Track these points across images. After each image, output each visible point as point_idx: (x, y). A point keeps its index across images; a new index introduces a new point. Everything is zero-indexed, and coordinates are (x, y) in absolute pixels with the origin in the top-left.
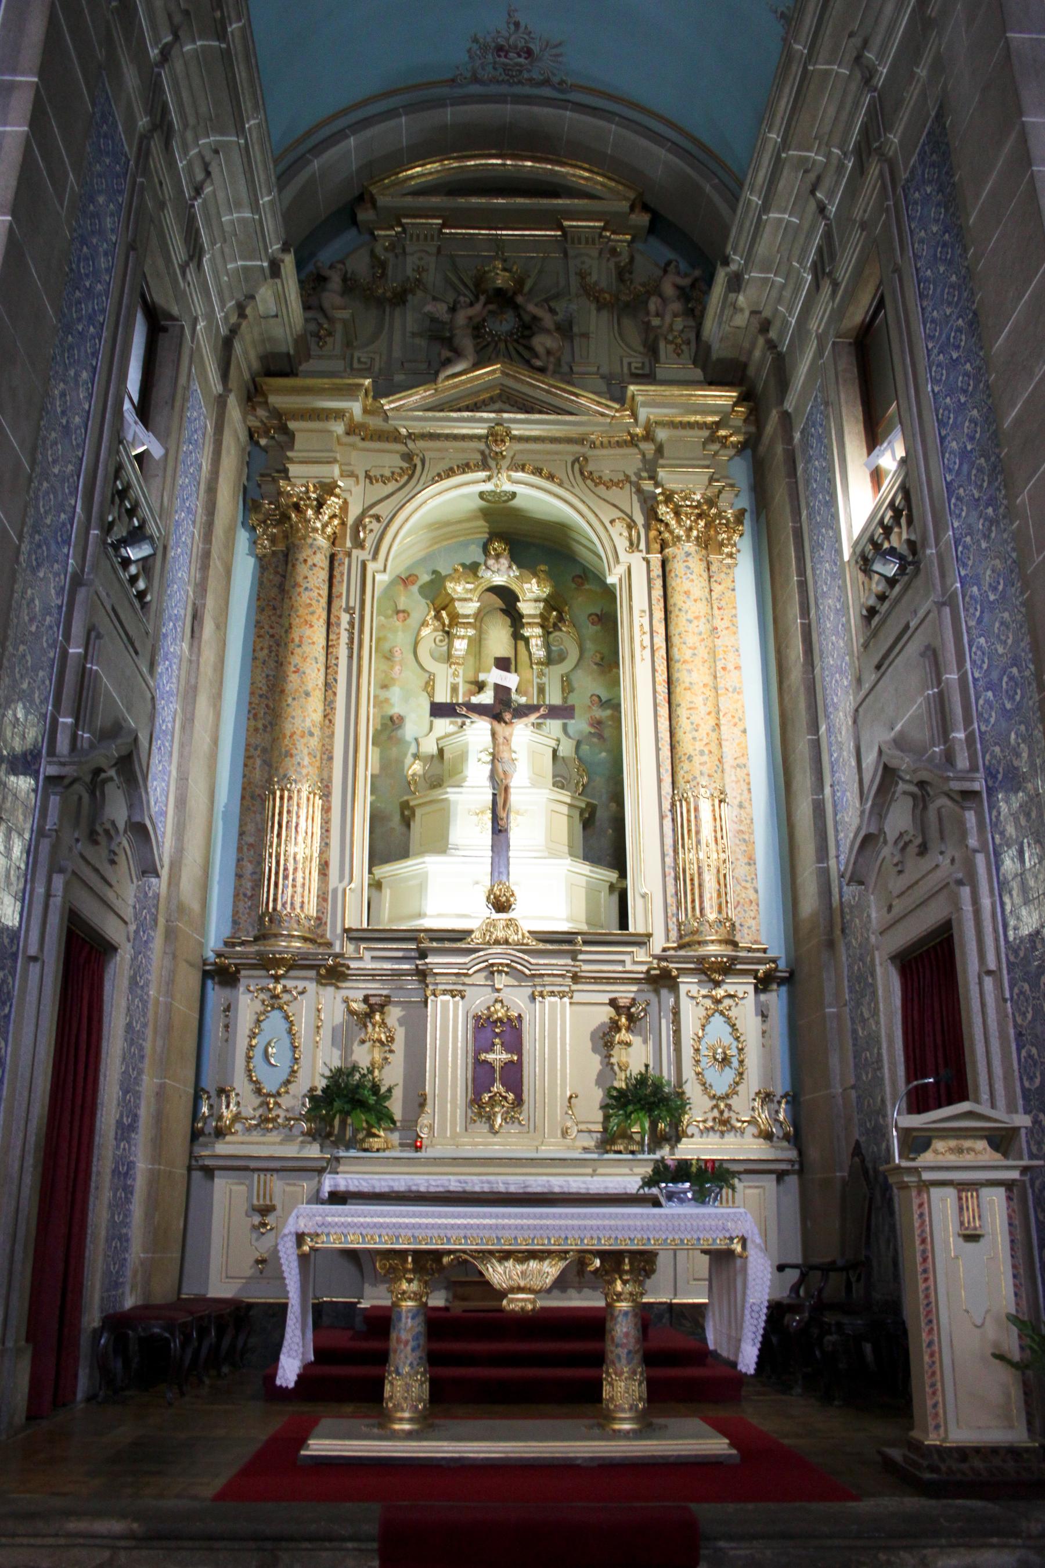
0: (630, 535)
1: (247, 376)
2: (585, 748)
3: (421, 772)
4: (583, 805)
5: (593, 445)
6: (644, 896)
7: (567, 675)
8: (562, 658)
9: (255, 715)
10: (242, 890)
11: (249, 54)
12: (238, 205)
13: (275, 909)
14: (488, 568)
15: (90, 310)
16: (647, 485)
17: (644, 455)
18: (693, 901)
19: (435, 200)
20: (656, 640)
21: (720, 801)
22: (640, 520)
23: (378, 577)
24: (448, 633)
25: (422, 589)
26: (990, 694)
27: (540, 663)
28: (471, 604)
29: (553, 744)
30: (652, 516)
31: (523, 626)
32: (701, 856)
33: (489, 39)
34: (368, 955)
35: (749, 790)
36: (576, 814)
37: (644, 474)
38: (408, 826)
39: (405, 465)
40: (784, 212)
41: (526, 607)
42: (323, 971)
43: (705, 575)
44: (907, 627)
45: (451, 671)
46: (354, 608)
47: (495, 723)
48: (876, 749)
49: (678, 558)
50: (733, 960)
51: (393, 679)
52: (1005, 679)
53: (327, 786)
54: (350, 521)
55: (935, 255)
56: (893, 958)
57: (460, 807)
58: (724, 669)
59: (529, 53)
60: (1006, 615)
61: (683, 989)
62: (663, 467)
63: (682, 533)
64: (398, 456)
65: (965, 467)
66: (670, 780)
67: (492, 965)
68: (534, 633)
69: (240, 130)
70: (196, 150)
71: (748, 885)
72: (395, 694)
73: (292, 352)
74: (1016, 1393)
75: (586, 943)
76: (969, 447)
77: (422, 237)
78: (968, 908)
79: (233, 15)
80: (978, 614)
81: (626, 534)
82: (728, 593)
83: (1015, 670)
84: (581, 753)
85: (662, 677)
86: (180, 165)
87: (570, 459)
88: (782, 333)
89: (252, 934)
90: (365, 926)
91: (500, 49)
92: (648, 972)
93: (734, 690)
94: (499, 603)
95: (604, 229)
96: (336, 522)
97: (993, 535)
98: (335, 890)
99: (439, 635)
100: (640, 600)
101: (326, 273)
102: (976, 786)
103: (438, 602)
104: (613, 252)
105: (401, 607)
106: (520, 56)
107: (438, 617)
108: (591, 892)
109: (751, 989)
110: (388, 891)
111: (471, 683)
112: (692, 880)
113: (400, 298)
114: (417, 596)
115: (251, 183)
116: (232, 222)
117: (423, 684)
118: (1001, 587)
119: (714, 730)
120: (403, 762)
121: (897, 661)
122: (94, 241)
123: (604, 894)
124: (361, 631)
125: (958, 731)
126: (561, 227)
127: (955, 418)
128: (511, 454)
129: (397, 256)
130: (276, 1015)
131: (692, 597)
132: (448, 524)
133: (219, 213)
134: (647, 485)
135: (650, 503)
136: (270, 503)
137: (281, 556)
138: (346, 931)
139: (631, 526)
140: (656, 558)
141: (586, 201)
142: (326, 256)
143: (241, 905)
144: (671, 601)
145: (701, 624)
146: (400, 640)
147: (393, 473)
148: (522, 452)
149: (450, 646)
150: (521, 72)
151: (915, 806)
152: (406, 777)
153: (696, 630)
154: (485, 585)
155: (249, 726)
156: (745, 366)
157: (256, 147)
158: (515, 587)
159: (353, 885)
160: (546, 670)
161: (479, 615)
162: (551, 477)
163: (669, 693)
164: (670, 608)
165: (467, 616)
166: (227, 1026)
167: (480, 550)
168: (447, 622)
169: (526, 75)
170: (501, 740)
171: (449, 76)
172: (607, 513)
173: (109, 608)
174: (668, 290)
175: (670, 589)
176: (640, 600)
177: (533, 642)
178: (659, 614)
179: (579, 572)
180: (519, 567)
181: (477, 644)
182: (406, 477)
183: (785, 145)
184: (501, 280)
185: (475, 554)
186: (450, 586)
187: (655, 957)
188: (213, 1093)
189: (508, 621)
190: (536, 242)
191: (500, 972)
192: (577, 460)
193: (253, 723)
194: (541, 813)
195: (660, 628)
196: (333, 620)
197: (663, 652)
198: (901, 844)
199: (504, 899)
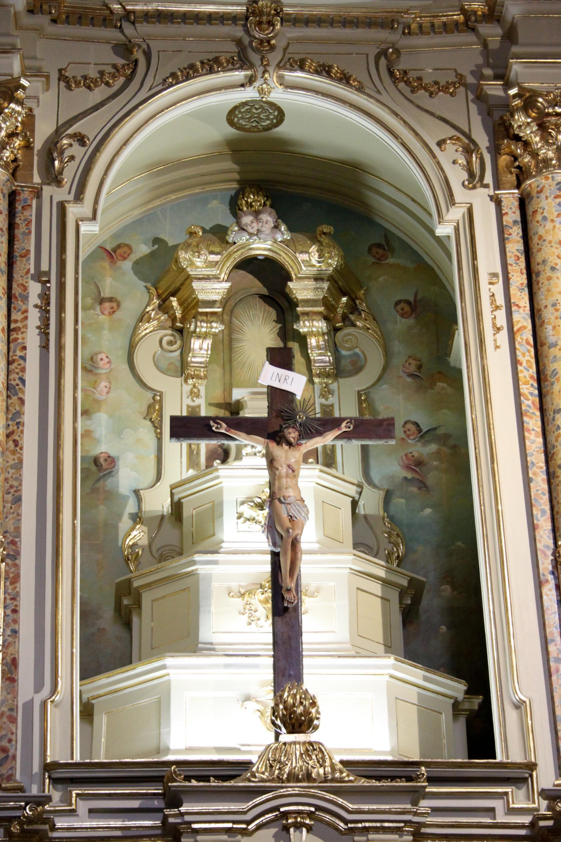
0: (469, 162)
2: (398, 502)
3: (145, 542)
4: (405, 583)
5: (407, 31)
6: (519, 706)
8: (357, 367)
14: (242, 229)
16: (494, 89)
17: (485, 45)
20: (516, 317)
22: (482, 140)
23: (85, 228)
24: (180, 331)
25: (138, 267)
27: (323, 374)
28: (217, 285)
29: (352, 490)
30: (502, 131)
31: (297, 318)
34: (83, 807)
36: (394, 596)
37: (488, 72)
38: (128, 625)
39: (120, 62)
41: (301, 290)
45: (187, 388)
46: (48, 274)
47: (273, 446)
49: (547, 192)
53: (13, 543)
54: (38, 144)
57: (215, 585)
62: (518, 56)
63: (551, 154)
64: (108, 47)
66: (549, 526)
67: (286, 815)
68: (313, 327)
72: (101, 422)
75: (433, 780)
81: (462, 161)
84: (393, 509)
85: (528, 372)
87: (373, 51)
90: (77, 758)
92: (533, 825)
94: (256, 285)
96: (18, 142)
98: (29, 705)
99: (167, 334)
100: (488, 259)
103: (163, 285)
105: (106, 293)
107: (164, 307)
108: (426, 712)
110: (104, 718)
111: (219, 406)
114: (131, 277)
117: (144, 408)
120: (116, 528)
123: (446, 717)
124: (61, 308)
128: (283, 44)
132: (180, 164)
134: (494, 89)
135: (497, 115)
138: (48, 767)
139: (470, 148)
140: (510, 197)
144: (538, 257)
146: (108, 343)
147: (102, 73)
148: (299, 40)
149: (185, 350)
152: (121, 549)
154: (237, 257)
158: (284, 258)
159: (57, 698)
160: (334, 386)
161: (230, 304)
162: (345, 79)
163: (541, 396)
164: (535, 268)
165: (212, 303)
167: (226, 209)
168: (178, 314)
170: (283, 470)
172: (434, 132)
175: (535, 240)
176: (488, 259)
177: (312, 341)
178: (519, 279)
180: (291, 229)
181: (226, 348)
182: (122, 80)
185: (219, 213)
186: (184, 256)
187: (544, 794)
189: (273, 313)
191: (298, 826)
192: (384, 53)
194: (339, 591)
195: (521, 299)
196: (16, 290)
197: (528, 335)
199: (300, 710)
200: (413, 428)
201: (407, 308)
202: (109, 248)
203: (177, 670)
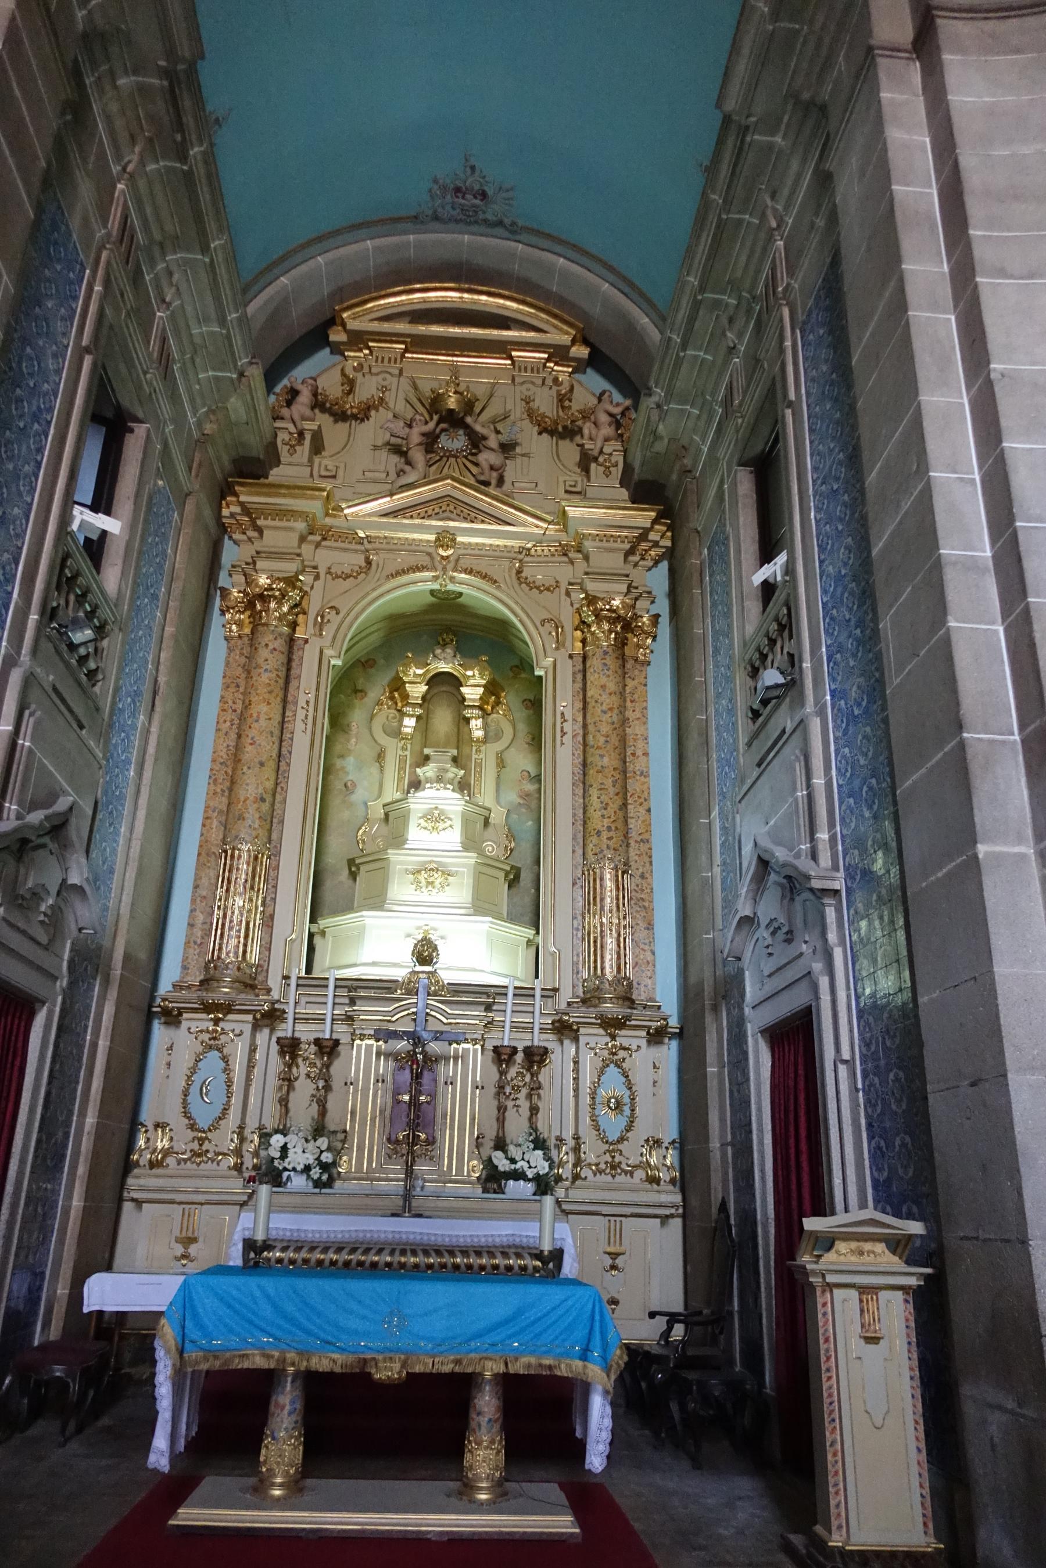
1: (219, 475)
2: (514, 816)
4: (508, 868)
7: (502, 752)
8: (498, 737)
9: (215, 780)
10: (193, 938)
11: (213, 178)
12: (207, 320)
13: (219, 957)
15: (34, 408)
18: (595, 961)
19: (401, 327)
21: (623, 873)
26: (851, 800)
32: (604, 920)
33: (448, 181)
35: (651, 863)
40: (700, 350)
42: (258, 1016)
43: (620, 672)
44: (784, 731)
45: (400, 745)
48: (752, 841)
49: (597, 655)
50: (628, 1018)
51: (350, 750)
52: (865, 789)
55: (823, 392)
56: (762, 1032)
58: (633, 754)
59: (484, 195)
60: (868, 729)
61: (583, 1040)
65: (839, 590)
69: (205, 249)
70: (165, 265)
71: (646, 947)
73: (262, 457)
76: (843, 572)
77: (386, 360)
78: (825, 998)
79: (194, 137)
80: (844, 725)
82: (641, 688)
83: (874, 781)
86: (147, 278)
88: (696, 462)
89: (199, 979)
91: (458, 190)
93: (642, 774)
95: (548, 360)
97: (860, 654)
101: (299, 387)
102: (836, 885)
104: (556, 380)
106: (475, 197)
109: (643, 1043)
112: (595, 942)
113: (363, 414)
115: (217, 299)
116: (202, 334)
118: (864, 703)
119: (620, 809)
121: (775, 762)
122: (41, 343)
125: (824, 833)
126: (511, 358)
127: (833, 545)
129: (364, 375)
130: (215, 1054)
131: (608, 691)
133: (188, 326)
136: (240, 592)
137: (246, 639)
141: (532, 334)
142: (300, 374)
143: (191, 951)
145: (615, 716)
149: (401, 721)
150: (476, 212)
151: (783, 897)
153: (610, 720)
155: (209, 789)
157: (222, 267)
166: (169, 1064)
169: (481, 216)
171: (413, 213)
173: (50, 690)
179: (516, 662)
180: (463, 656)
183: (702, 289)
184: (452, 403)
188: (151, 1127)
190: (488, 370)
193: (212, 787)
198: (772, 929)
200: (526, 774)
201: (529, 704)
202: (363, 660)
203: (370, 919)
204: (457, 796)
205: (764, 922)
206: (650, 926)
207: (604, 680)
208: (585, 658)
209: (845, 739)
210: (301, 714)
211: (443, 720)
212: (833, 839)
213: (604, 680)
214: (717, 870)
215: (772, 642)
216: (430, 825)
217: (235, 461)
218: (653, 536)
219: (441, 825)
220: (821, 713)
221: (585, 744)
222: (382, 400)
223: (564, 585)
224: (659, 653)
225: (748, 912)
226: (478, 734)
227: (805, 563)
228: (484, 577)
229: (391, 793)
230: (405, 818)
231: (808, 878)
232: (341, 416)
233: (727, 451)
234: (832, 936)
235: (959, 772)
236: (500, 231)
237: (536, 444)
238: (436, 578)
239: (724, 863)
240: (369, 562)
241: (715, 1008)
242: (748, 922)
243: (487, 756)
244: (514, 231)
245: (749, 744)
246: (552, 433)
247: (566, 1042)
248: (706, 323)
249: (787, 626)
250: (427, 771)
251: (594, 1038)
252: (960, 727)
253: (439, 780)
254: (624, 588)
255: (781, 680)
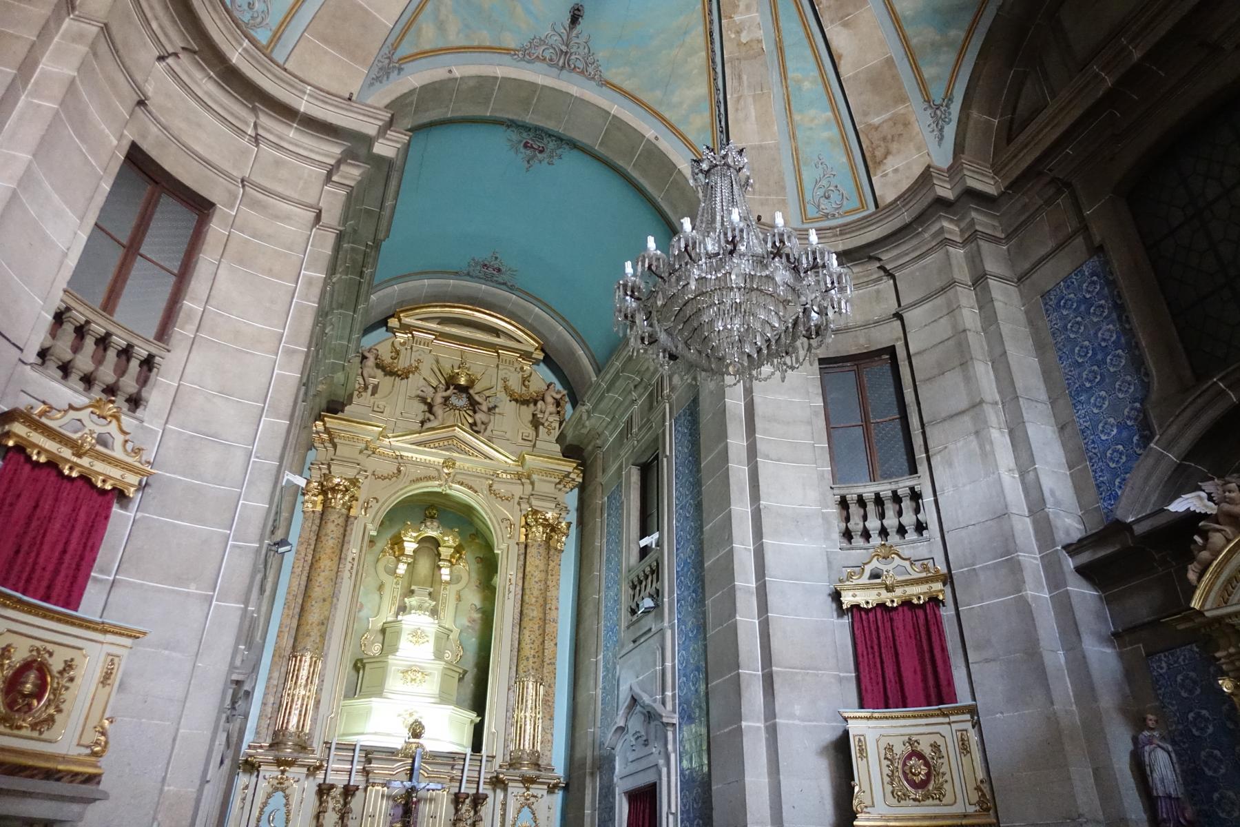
19: (433, 326)
50: (538, 777)
59: (499, 270)
61: (510, 790)
74: (1119, 676)
78: (664, 779)
101: (367, 354)
104: (522, 368)
109: (545, 792)
113: (405, 375)
130: (281, 793)
156: (582, 450)
174: (549, 399)
203: (375, 702)
204: (431, 620)
205: (631, 731)
206: (551, 719)
207: (537, 562)
208: (526, 546)
209: (683, 646)
210: (349, 566)
211: (424, 566)
212: (674, 696)
213: (537, 562)
214: (599, 691)
215: (646, 577)
216: (414, 639)
217: (328, 402)
218: (572, 476)
219: (421, 641)
220: (672, 627)
221: (522, 600)
222: (417, 368)
223: (517, 499)
224: (568, 544)
225: (622, 724)
226: (446, 578)
227: (667, 539)
228: (470, 488)
229: (387, 615)
230: (398, 634)
231: (661, 716)
232: (389, 372)
233: (625, 453)
234: (670, 747)
235: (736, 683)
236: (504, 287)
237: (508, 407)
238: (441, 485)
239: (604, 688)
240: (399, 471)
241: (592, 774)
242: (621, 729)
243: (449, 594)
244: (512, 289)
245: (628, 627)
246: (516, 401)
247: (498, 791)
248: (620, 384)
249: (656, 571)
250: (412, 601)
251: (515, 789)
252: (738, 667)
253: (420, 608)
254: (553, 506)
255: (652, 604)
